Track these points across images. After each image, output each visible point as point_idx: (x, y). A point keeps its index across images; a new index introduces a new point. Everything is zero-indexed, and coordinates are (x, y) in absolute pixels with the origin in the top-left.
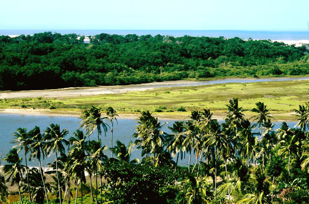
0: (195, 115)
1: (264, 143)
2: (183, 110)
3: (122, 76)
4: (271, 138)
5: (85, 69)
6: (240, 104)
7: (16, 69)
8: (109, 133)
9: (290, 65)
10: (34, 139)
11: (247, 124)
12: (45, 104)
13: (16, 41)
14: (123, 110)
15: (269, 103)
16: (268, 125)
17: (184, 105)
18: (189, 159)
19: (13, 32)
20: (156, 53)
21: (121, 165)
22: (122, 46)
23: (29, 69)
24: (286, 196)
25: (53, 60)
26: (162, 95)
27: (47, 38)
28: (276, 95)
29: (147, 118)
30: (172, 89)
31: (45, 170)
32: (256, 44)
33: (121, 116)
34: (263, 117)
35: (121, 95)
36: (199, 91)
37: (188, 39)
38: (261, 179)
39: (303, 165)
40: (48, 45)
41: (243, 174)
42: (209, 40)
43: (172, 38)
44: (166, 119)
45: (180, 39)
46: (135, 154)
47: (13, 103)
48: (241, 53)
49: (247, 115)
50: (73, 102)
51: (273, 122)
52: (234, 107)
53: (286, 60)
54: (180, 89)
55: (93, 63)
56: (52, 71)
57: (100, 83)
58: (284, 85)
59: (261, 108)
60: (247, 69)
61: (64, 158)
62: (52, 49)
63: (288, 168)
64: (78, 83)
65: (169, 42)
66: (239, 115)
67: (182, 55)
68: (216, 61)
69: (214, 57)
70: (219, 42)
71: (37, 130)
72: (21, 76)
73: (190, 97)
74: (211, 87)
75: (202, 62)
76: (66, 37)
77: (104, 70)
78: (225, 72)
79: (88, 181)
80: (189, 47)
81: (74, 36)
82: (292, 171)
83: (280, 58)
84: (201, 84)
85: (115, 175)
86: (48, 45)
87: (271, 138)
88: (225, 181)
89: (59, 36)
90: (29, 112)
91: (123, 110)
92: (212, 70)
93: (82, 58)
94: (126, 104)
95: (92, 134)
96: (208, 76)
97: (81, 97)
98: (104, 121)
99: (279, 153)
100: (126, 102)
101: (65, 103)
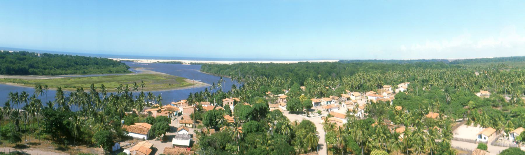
0: (78, 90)
1: (104, 101)
2: (75, 87)
3: (52, 72)
4: (107, 99)
5: (38, 68)
6: (95, 85)
7: (12, 66)
8: (45, 96)
9: (115, 69)
10: (17, 97)
11: (97, 94)
12: (21, 82)
13: (12, 54)
14: (52, 86)
15: (106, 85)
16: (105, 94)
17: (75, 85)
18: (75, 108)
19: (11, 49)
20: (65, 62)
22: (52, 59)
23: (16, 67)
24: (112, 124)
25: (26, 63)
26: (67, 80)
27: (24, 53)
28: (109, 81)
29: (60, 90)
30: (71, 78)
31: (20, 111)
33: (50, 89)
34: (103, 91)
35: (51, 80)
36: (81, 79)
37: (77, 57)
38: (102, 117)
39: (118, 111)
40: (24, 56)
41: (95, 115)
42: (85, 58)
43: (71, 56)
44: (67, 91)
45: (74, 57)
46: (55, 106)
48: (97, 64)
49: (98, 90)
50: (33, 82)
51: (107, 93)
52: (93, 87)
53: (113, 67)
54: (74, 78)
55: (41, 65)
56: (25, 68)
57: (43, 74)
58: (112, 77)
59: (103, 87)
60: (99, 70)
61: (27, 106)
62: (25, 59)
63: (113, 112)
64: (35, 74)
65: (70, 58)
66: (94, 90)
67: (75, 63)
68: (88, 67)
69: (87, 65)
70: (88, 59)
71: (17, 94)
72: (13, 70)
73: (78, 82)
74: (86, 78)
75: (82, 67)
76: (31, 54)
77: (45, 69)
78: (91, 72)
79: (36, 117)
80: (78, 60)
81: (34, 53)
82: (114, 113)
83: (112, 66)
84: (82, 76)
85: (46, 115)
86: (24, 56)
87: (107, 99)
88: (89, 119)
89: (28, 53)
90: (16, 85)
91: (52, 86)
92: (86, 71)
93: (37, 63)
94: (53, 84)
95: (38, 96)
96: (84, 73)
97: (36, 80)
98: (44, 91)
99: (109, 105)
100: (52, 82)
101: (30, 82)
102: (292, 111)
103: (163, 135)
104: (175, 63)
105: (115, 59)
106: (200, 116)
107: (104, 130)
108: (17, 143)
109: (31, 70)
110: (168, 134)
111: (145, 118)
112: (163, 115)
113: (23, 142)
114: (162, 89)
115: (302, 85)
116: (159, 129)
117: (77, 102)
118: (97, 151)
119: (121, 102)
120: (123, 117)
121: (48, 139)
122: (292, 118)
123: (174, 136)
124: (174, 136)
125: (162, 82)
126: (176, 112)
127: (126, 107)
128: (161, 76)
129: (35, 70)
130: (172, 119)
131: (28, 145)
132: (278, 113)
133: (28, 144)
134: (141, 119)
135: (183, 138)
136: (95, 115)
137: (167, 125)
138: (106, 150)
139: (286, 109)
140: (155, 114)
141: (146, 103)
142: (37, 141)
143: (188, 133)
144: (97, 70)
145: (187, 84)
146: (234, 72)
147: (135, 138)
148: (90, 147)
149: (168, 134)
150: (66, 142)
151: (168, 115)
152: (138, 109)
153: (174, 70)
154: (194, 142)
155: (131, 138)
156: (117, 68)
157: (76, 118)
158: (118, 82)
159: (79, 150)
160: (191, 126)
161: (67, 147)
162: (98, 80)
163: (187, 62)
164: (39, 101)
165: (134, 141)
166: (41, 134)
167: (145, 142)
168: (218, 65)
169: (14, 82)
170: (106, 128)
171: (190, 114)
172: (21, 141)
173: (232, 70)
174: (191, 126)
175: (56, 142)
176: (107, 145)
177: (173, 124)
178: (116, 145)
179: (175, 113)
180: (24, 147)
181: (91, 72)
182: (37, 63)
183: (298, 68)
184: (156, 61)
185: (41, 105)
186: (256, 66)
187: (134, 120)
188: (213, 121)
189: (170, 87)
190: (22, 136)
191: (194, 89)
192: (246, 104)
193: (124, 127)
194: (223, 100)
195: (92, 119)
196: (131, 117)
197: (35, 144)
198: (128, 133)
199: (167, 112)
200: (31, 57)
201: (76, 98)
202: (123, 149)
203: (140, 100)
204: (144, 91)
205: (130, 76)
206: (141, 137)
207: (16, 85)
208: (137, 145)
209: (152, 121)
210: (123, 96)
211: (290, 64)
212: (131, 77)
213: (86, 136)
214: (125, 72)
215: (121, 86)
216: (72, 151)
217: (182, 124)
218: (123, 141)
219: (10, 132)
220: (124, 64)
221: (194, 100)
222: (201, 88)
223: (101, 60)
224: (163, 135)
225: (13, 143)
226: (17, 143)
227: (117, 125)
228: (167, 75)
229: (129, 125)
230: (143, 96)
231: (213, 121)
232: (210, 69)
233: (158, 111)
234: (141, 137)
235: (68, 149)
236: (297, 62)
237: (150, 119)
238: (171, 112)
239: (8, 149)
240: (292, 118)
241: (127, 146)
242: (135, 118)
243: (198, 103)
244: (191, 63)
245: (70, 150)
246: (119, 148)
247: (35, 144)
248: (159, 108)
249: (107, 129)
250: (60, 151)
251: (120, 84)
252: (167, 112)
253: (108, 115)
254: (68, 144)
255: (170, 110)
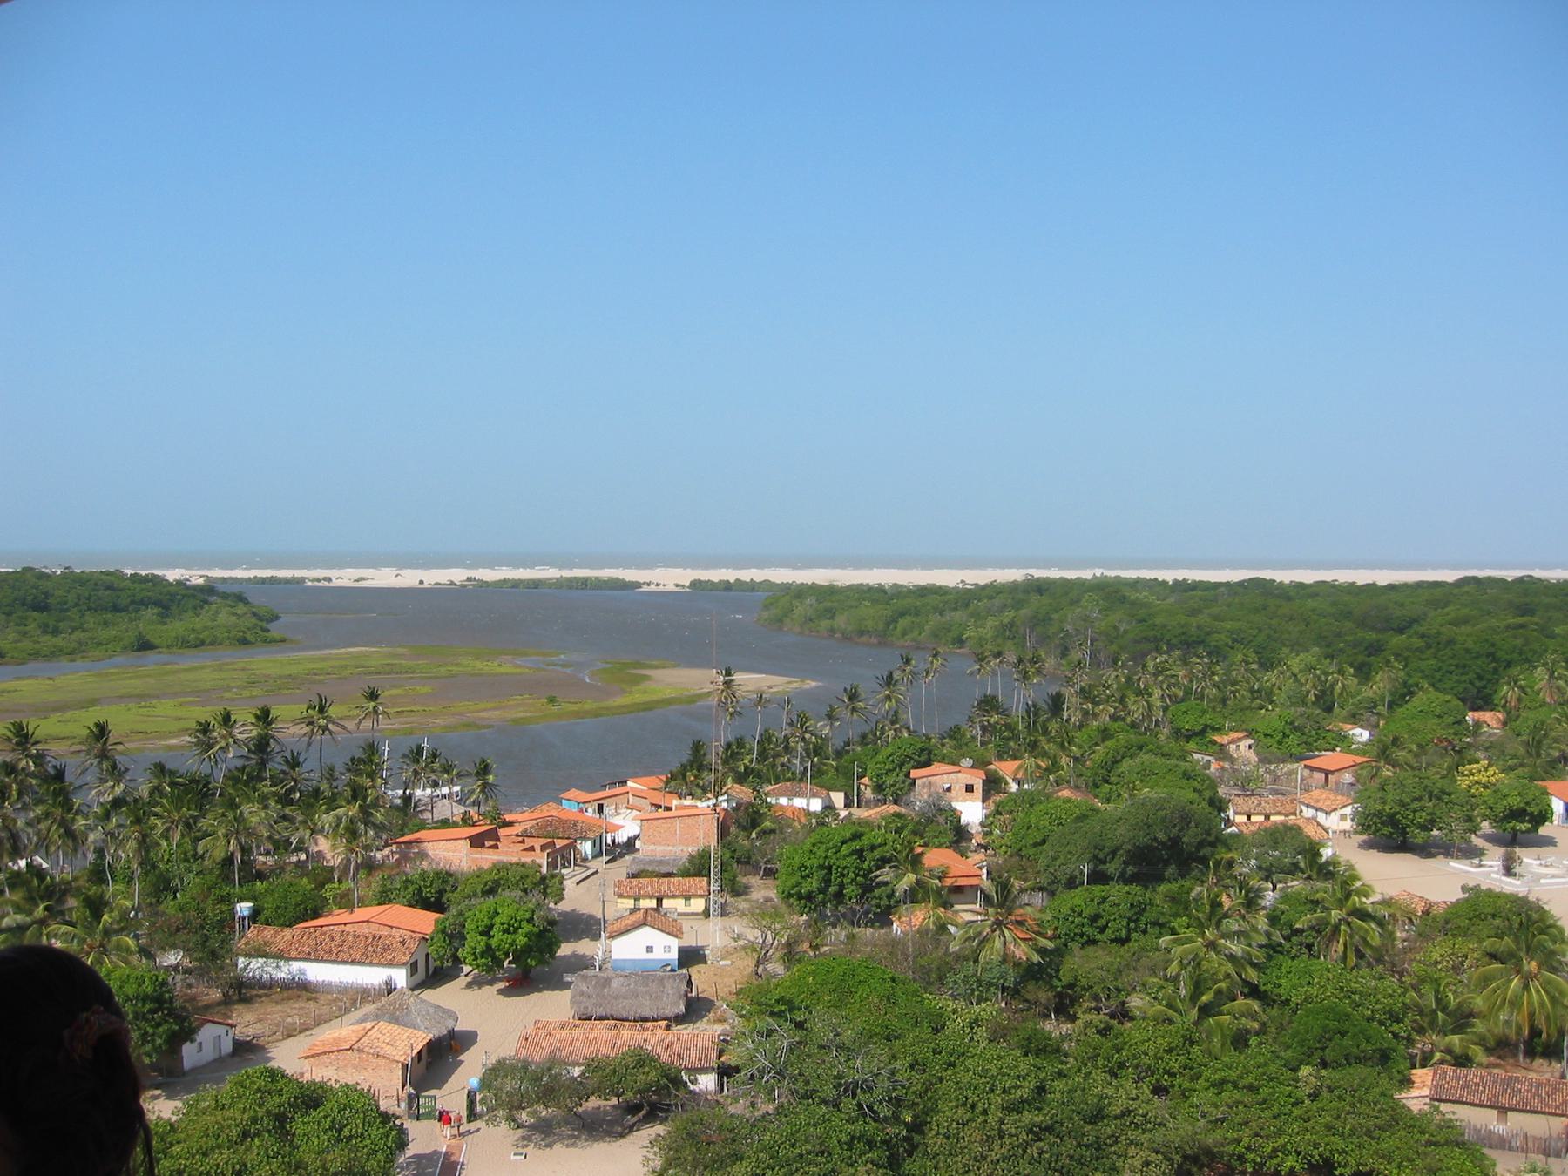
9: (177, 627)
15: (120, 720)
16: (116, 773)
21: (38, 858)
32: (82, 580)
47: (997, 602)
48: (41, 607)
83: (151, 613)
102: (1391, 832)
104: (584, 583)
105: (172, 575)
115: (1483, 701)
122: (1391, 878)
126: (598, 842)
132: (1306, 857)
139: (1348, 825)
146: (989, 627)
147: (327, 988)
151: (542, 860)
168: (880, 589)
173: (976, 615)
174: (698, 905)
183: (1452, 611)
184: (458, 575)
186: (1141, 596)
188: (844, 884)
192: (1066, 793)
194: (914, 774)
206: (372, 976)
211: (1391, 587)
223: (74, 580)
231: (844, 884)
232: (831, 613)
234: (372, 976)
236: (1450, 576)
240: (1391, 878)
243: (744, 793)
244: (696, 584)
251: (219, 709)
255: (548, 830)
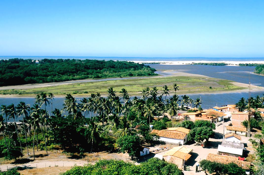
0: (93, 96)
3: (56, 78)
5: (37, 75)
6: (114, 90)
9: (137, 72)
11: (117, 98)
15: (128, 89)
17: (87, 90)
20: (73, 67)
22: (55, 64)
26: (76, 86)
29: (69, 97)
30: (81, 83)
33: (56, 97)
34: (125, 95)
36: (94, 84)
37: (88, 61)
39: (145, 115)
40: (17, 64)
41: (117, 120)
42: (98, 61)
43: (80, 60)
44: (78, 97)
46: (64, 113)
48: (113, 67)
49: (117, 94)
50: (31, 91)
52: (111, 92)
53: (135, 70)
55: (40, 72)
59: (124, 91)
60: (117, 74)
66: (114, 95)
67: (85, 68)
68: (102, 71)
69: (101, 69)
70: (103, 62)
73: (90, 87)
74: (100, 82)
75: (95, 71)
76: (26, 61)
80: (89, 64)
83: (132, 69)
84: (95, 81)
86: (17, 64)
88: (108, 124)
90: (8, 96)
91: (57, 93)
92: (100, 75)
93: (35, 70)
94: (59, 91)
95: (42, 106)
96: (98, 77)
97: (35, 88)
98: (49, 100)
99: (133, 110)
100: (59, 90)
101: (27, 91)
103: (205, 140)
105: (136, 62)
106: (257, 124)
107: (129, 134)
108: (17, 158)
109: (28, 78)
110: (210, 140)
111: (181, 123)
112: (205, 120)
113: (26, 156)
114: (200, 92)
116: (199, 134)
117: (93, 108)
118: (121, 156)
119: (148, 106)
120: (151, 121)
121: (57, 149)
123: (220, 143)
124: (220, 143)
125: (200, 84)
127: (155, 110)
128: (199, 78)
129: (33, 78)
130: (217, 124)
131: (32, 159)
133: (31, 157)
134: (174, 123)
135: (233, 145)
136: (117, 120)
137: (211, 130)
138: (132, 156)
140: (193, 118)
141: (180, 107)
142: (44, 152)
143: (240, 142)
144: (114, 74)
145: (235, 87)
148: (111, 152)
149: (210, 140)
150: (81, 150)
152: (170, 114)
153: (216, 70)
154: (248, 152)
155: (163, 143)
156: (140, 71)
157: (93, 124)
158: (142, 85)
159: (97, 156)
160: (244, 134)
161: (82, 155)
162: (115, 84)
163: (235, 63)
164: (44, 112)
165: (167, 146)
166: (48, 144)
167: (181, 147)
169: (4, 94)
170: (130, 133)
171: (243, 121)
172: (22, 155)
175: (67, 151)
176: (134, 150)
177: (218, 130)
178: (145, 150)
179: (219, 119)
180: (27, 161)
181: (106, 76)
182: (35, 70)
184: (190, 62)
185: (47, 117)
187: (166, 124)
189: (210, 90)
190: (23, 149)
191: (244, 94)
193: (153, 131)
195: (112, 124)
196: (162, 121)
197: (41, 156)
198: (159, 137)
199: (210, 117)
200: (26, 64)
201: (90, 104)
202: (154, 154)
203: (173, 104)
204: (178, 95)
205: (157, 79)
207: (8, 96)
208: (171, 150)
209: (190, 126)
210: (150, 99)
212: (158, 80)
213: (106, 142)
214: (149, 75)
215: (148, 89)
216: (89, 158)
217: (230, 130)
218: (152, 146)
219: (5, 148)
220: (148, 67)
221: (248, 105)
222: (255, 93)
224: (205, 140)
225: (11, 159)
226: (17, 158)
227: (144, 131)
228: (207, 78)
229: (160, 129)
230: (176, 100)
233: (197, 115)
234: (177, 142)
235: (84, 156)
237: (187, 123)
238: (214, 117)
239: (6, 166)
241: (158, 150)
242: (168, 123)
243: (253, 110)
245: (86, 158)
246: (148, 153)
247: (41, 156)
248: (199, 112)
249: (133, 134)
250: (74, 159)
252: (210, 117)
253: (133, 120)
254: (84, 152)
